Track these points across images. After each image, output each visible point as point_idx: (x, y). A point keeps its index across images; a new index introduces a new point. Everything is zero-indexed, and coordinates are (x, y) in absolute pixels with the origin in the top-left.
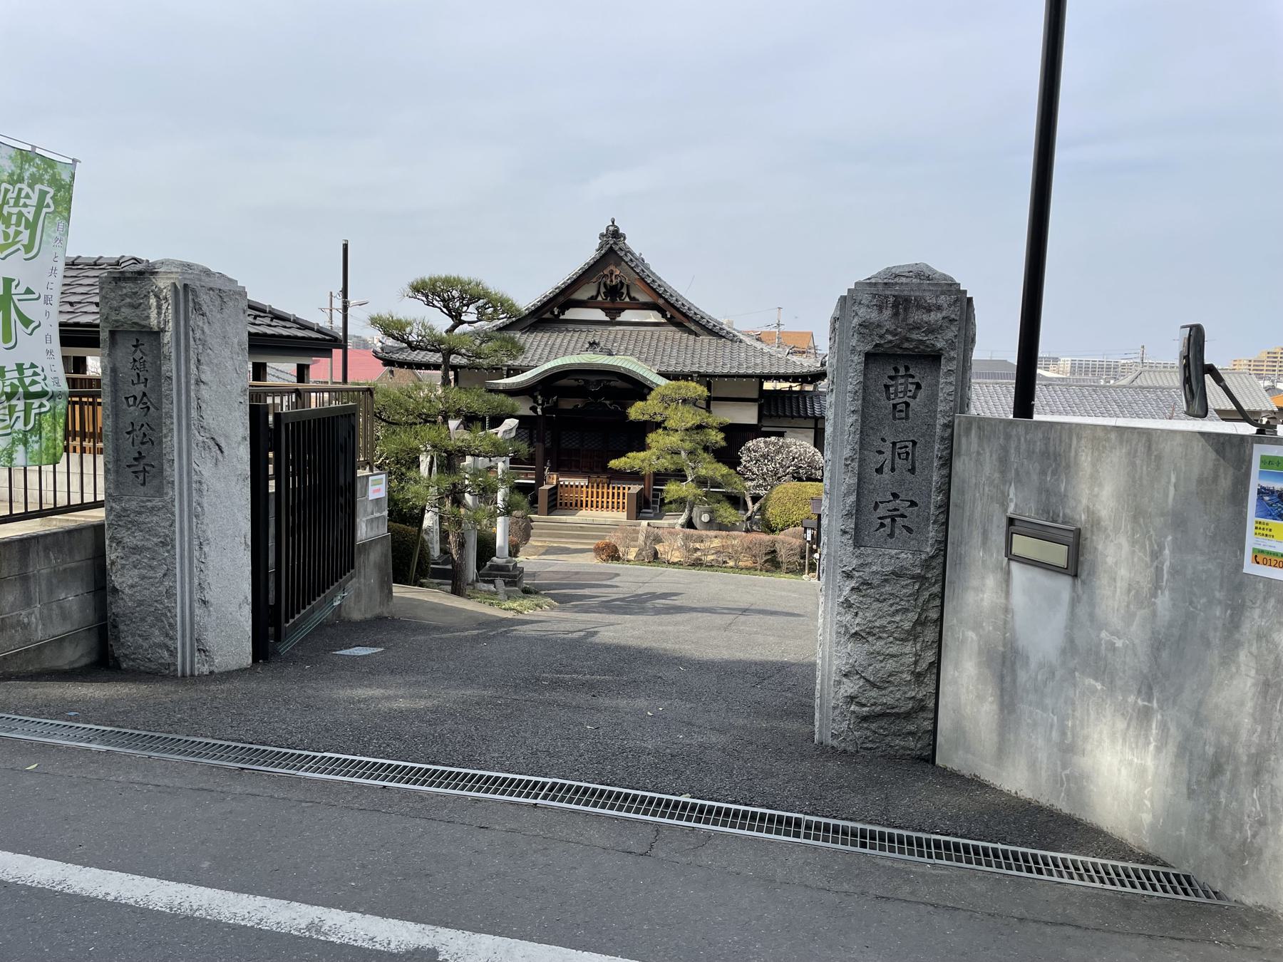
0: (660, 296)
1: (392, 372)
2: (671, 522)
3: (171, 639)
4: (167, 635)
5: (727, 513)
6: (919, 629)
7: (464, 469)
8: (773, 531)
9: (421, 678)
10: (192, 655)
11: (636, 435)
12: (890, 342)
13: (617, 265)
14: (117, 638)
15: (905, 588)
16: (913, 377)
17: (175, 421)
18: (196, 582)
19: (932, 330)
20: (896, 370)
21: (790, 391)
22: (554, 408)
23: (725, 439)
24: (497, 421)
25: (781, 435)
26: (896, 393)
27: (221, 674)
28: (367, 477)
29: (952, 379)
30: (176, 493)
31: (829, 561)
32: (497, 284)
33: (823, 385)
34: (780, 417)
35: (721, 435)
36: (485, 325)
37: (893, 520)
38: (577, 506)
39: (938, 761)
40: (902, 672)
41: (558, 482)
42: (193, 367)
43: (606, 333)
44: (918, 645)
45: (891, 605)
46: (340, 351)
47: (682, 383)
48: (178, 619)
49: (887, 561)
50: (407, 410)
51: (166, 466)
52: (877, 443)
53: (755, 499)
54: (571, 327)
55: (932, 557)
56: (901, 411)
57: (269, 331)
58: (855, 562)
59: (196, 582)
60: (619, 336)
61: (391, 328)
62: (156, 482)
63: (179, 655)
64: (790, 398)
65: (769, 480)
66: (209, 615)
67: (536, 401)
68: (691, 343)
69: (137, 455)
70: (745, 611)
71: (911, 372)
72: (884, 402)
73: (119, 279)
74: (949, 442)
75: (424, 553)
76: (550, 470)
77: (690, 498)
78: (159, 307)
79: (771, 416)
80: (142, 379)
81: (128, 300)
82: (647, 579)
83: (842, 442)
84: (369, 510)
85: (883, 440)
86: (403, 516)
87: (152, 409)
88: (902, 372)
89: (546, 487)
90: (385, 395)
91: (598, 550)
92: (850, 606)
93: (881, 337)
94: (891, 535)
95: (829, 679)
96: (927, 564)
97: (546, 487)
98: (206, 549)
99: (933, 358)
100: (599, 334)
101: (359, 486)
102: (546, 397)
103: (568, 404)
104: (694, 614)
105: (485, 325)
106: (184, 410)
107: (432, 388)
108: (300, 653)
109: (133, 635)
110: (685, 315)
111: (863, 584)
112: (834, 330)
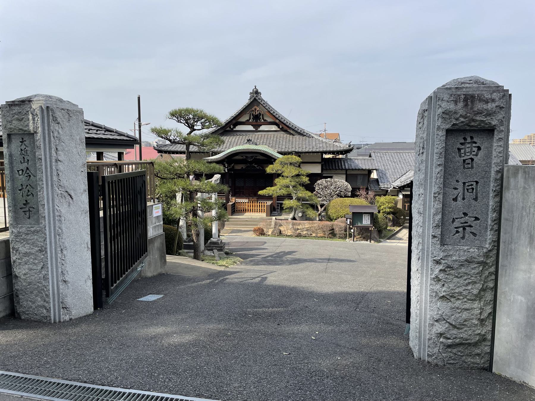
0: (277, 118)
1: (161, 155)
2: (286, 217)
3: (47, 302)
4: (45, 301)
5: (311, 213)
6: (482, 293)
7: (197, 199)
8: (332, 220)
9: (184, 316)
10: (59, 311)
11: (269, 180)
12: (462, 122)
13: (258, 106)
14: (18, 302)
15: (474, 270)
16: (475, 143)
17: (44, 182)
18: (60, 270)
19: (489, 114)
20: (465, 139)
23: (309, 180)
24: (210, 176)
25: (331, 177)
26: (465, 153)
27: (76, 319)
28: (152, 206)
29: (501, 143)
32: (210, 111)
33: (349, 155)
34: (330, 169)
35: (308, 178)
36: (206, 131)
37: (464, 229)
38: (244, 211)
39: (494, 370)
40: (472, 319)
41: (235, 201)
42: (53, 153)
43: (254, 136)
44: (482, 303)
45: (465, 280)
46: (138, 146)
47: (289, 156)
48: (51, 292)
49: (462, 253)
50: (170, 172)
51: (41, 208)
53: (322, 206)
54: (238, 133)
55: (490, 251)
56: (468, 163)
57: (104, 137)
58: (442, 255)
59: (60, 270)
60: (260, 137)
61: (161, 133)
62: (36, 217)
63: (52, 311)
64: (335, 161)
66: (68, 288)
68: (291, 139)
69: (25, 202)
70: (329, 260)
71: (475, 140)
72: (458, 158)
73: (12, 105)
74: (500, 181)
75: (180, 238)
77: (295, 206)
78: (34, 119)
79: (326, 169)
80: (26, 160)
81: (16, 116)
82: (279, 244)
83: (431, 183)
84: (154, 222)
85: (457, 181)
86: (169, 221)
87: (32, 176)
88: (469, 140)
90: (159, 165)
91: (255, 231)
92: (439, 280)
94: (463, 238)
95: (425, 322)
96: (487, 255)
98: (65, 252)
99: (490, 131)
100: (251, 136)
101: (148, 210)
102: (229, 164)
103: (238, 167)
104: (307, 264)
105: (206, 131)
106: (49, 177)
107: (181, 161)
108: (120, 301)
109: (27, 301)
110: (288, 127)
111: (448, 267)
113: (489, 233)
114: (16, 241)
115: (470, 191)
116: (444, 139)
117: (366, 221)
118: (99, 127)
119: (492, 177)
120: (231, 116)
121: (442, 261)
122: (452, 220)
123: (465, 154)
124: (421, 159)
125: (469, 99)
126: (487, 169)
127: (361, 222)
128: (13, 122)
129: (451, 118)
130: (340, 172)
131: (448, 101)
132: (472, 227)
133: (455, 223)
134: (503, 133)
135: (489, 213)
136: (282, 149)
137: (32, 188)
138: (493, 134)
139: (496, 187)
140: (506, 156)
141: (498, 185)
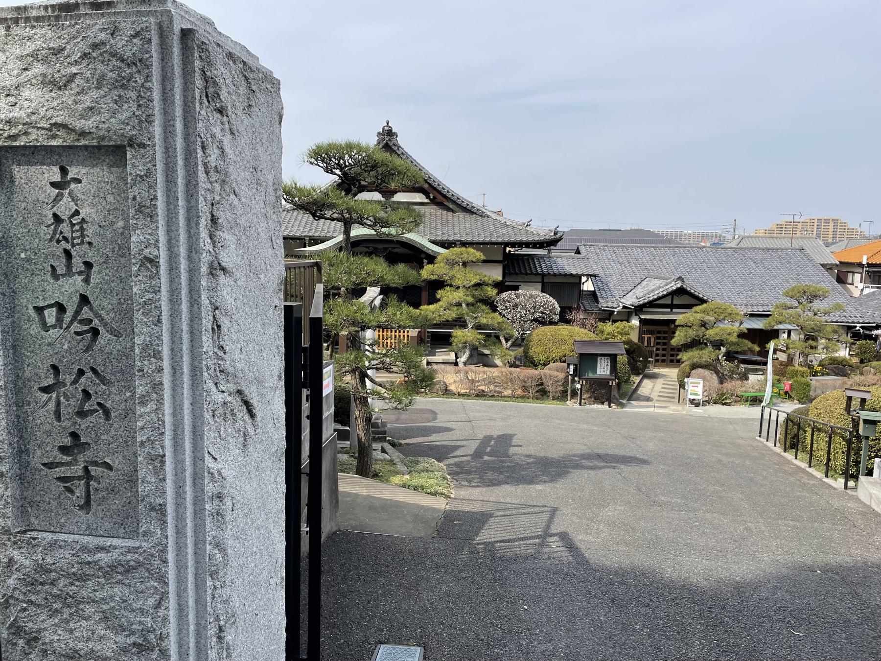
17: (166, 364)
30: (171, 532)
34: (517, 274)
62: (116, 503)
68: (450, 218)
69: (68, 441)
79: (510, 274)
87: (105, 337)
114: (30, 602)
117: (603, 369)
127: (595, 371)
128: (26, 93)
130: (533, 278)
137: (103, 380)
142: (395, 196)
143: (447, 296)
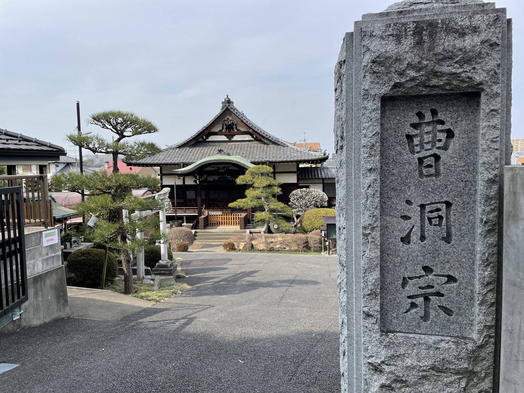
0: (250, 128)
5: (285, 225)
11: (240, 191)
12: (413, 79)
13: (230, 115)
16: (442, 123)
19: (469, 59)
20: (420, 115)
21: (311, 167)
22: (206, 180)
23: (282, 191)
25: (308, 187)
29: (496, 121)
31: (350, 344)
33: (325, 164)
34: (307, 179)
35: (280, 189)
37: (427, 299)
38: (218, 224)
43: (227, 146)
47: (260, 166)
49: (424, 352)
52: (402, 206)
53: (298, 217)
54: (211, 144)
55: (481, 347)
58: (383, 354)
60: (233, 147)
64: (311, 171)
65: (304, 208)
67: (196, 178)
68: (265, 148)
70: (292, 282)
71: (441, 116)
72: (407, 156)
76: (205, 209)
79: (303, 179)
83: (358, 206)
85: (409, 202)
88: (428, 117)
89: (203, 217)
91: (225, 246)
93: (401, 74)
94: (425, 317)
96: (474, 357)
97: (203, 217)
99: (470, 96)
100: (223, 146)
102: (201, 176)
110: (262, 136)
111: (396, 381)
112: (339, 78)
113: (476, 309)
115: (435, 221)
116: (378, 116)
118: (13, 136)
119: (479, 193)
120: (203, 126)
121: (384, 366)
122: (400, 282)
123: (422, 147)
124: (339, 160)
125: (425, 31)
126: (469, 177)
129: (390, 72)
130: (317, 181)
131: (382, 38)
132: (442, 295)
133: (407, 288)
134: (499, 99)
135: (476, 267)
136: (256, 159)
138: (478, 104)
139: (489, 213)
140: (507, 149)
141: (493, 210)
142: (234, 137)
143: (249, 193)
